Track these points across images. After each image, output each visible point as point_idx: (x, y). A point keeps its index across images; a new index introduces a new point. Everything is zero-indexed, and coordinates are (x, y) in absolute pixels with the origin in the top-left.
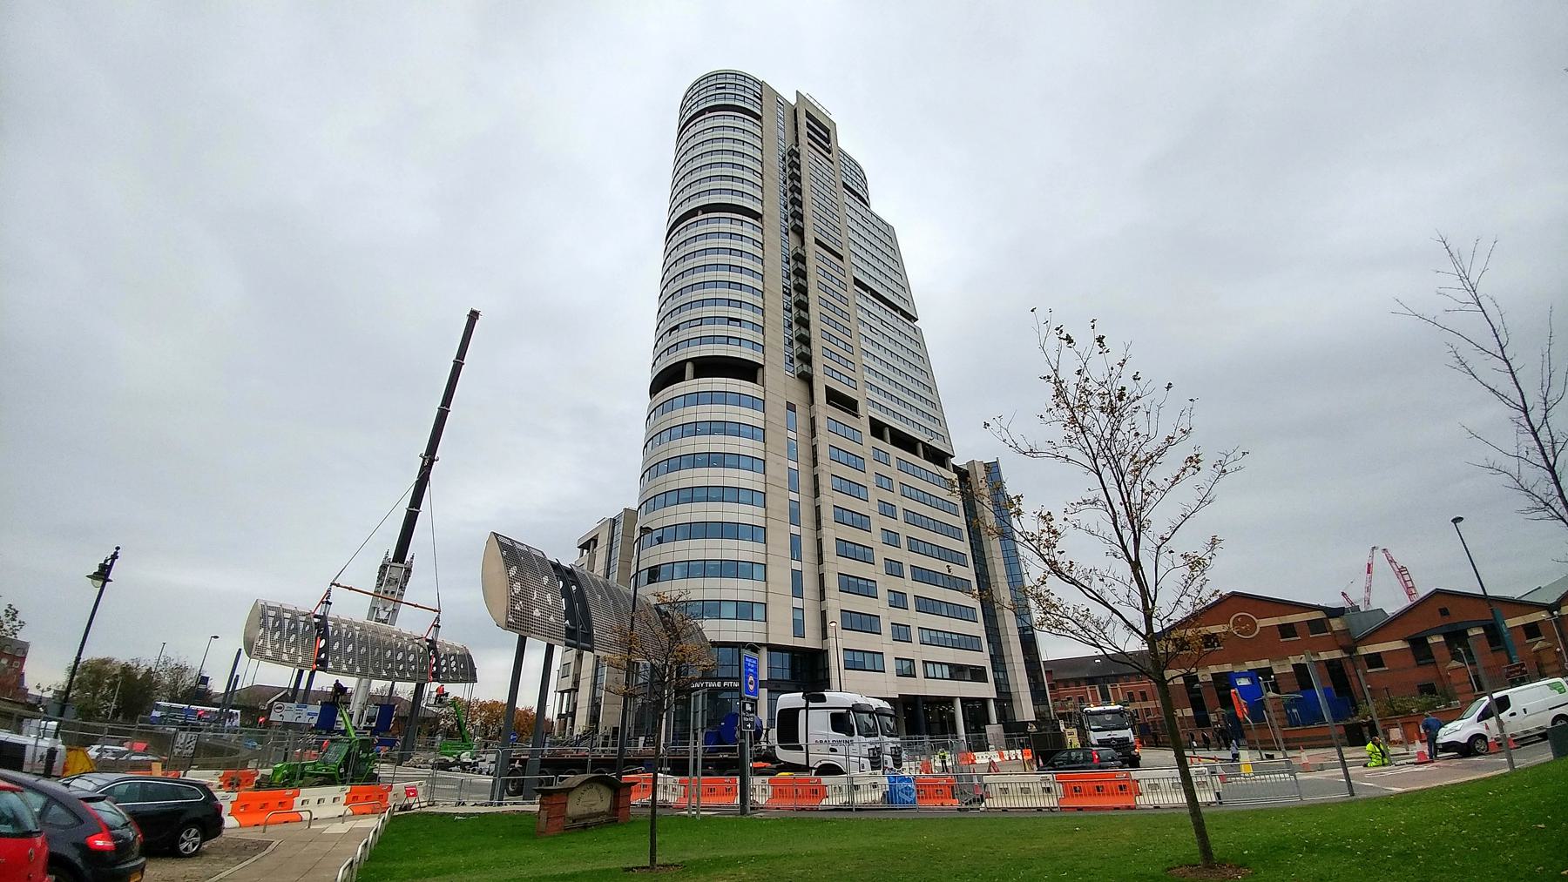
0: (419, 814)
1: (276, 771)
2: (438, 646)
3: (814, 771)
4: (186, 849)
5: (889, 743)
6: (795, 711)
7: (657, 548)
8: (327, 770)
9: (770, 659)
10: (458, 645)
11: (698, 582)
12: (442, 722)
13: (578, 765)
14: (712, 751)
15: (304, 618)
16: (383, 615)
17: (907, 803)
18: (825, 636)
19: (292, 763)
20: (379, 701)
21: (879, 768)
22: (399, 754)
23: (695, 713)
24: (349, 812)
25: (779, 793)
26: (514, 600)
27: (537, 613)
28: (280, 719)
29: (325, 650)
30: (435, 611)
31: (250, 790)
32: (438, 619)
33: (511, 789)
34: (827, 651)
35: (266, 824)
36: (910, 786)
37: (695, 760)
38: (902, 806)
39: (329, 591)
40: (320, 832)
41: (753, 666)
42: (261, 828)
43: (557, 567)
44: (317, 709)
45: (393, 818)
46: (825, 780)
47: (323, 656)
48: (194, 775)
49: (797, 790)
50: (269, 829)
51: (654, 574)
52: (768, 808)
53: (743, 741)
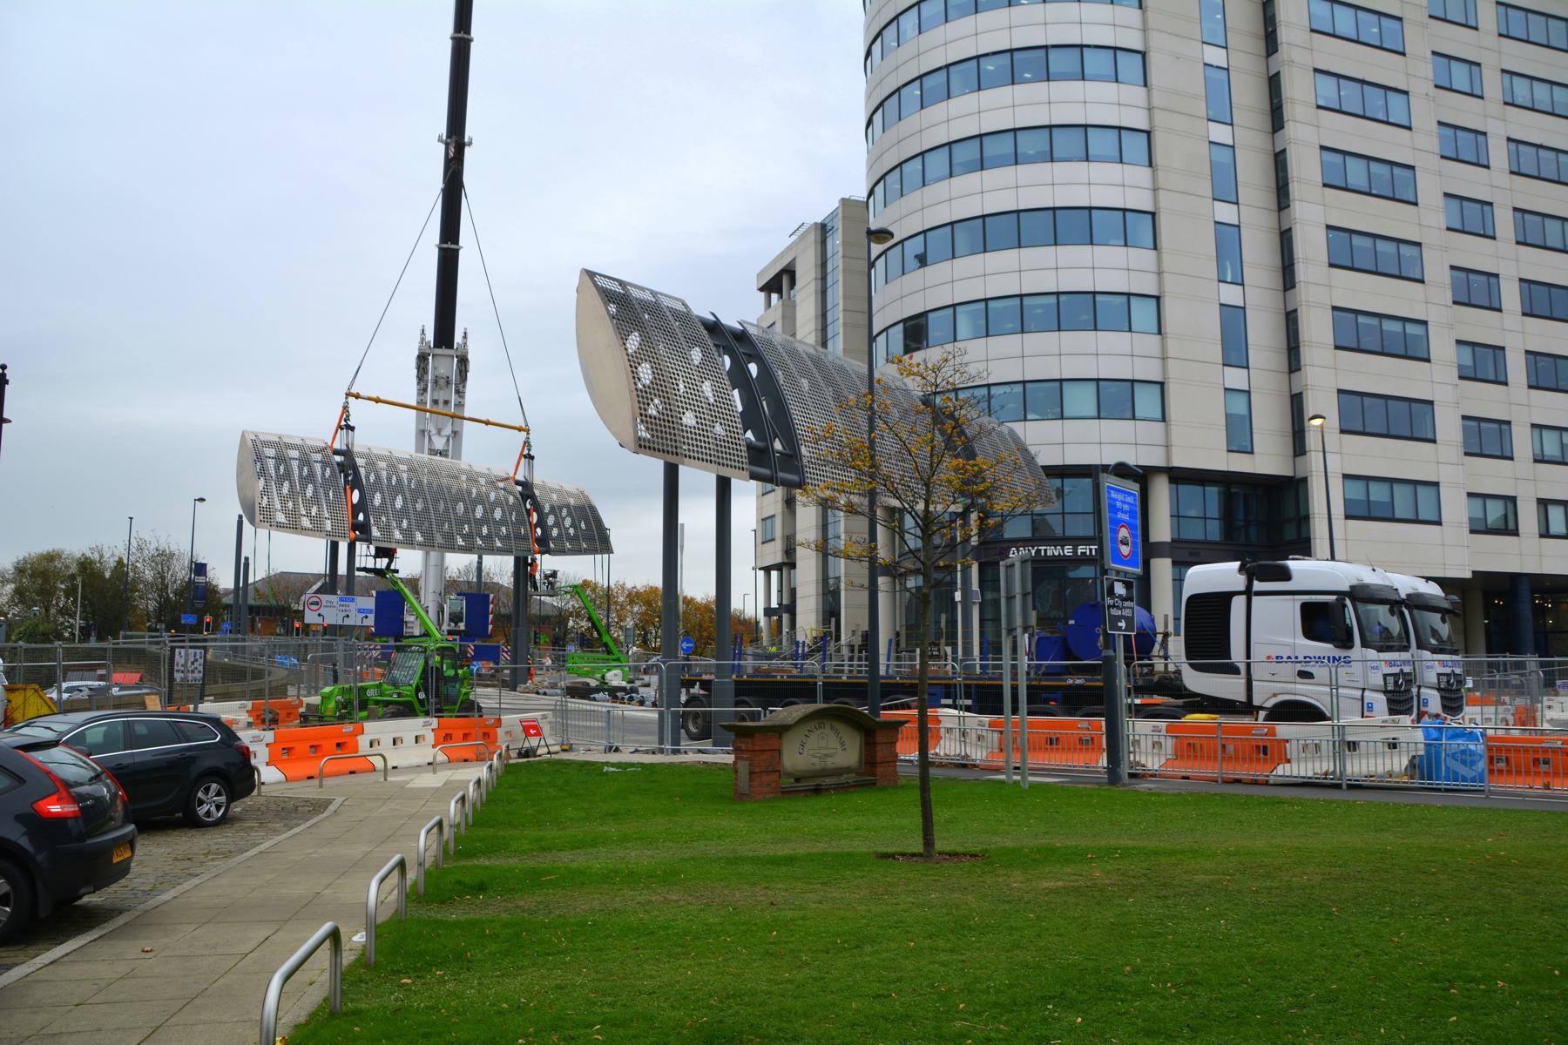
0: (548, 762)
1: (325, 698)
2: (537, 492)
3: (1262, 714)
4: (208, 814)
5: (1432, 667)
6: (1224, 599)
7: (918, 277)
8: (399, 695)
9: (1176, 502)
10: (570, 487)
11: (1010, 343)
12: (571, 623)
13: (799, 690)
14: (1051, 672)
15: (318, 457)
16: (439, 443)
17: (1464, 779)
18: (1299, 444)
19: (347, 686)
20: (465, 589)
21: (1408, 712)
22: (741, 656)
23: (1010, 598)
24: (441, 757)
25: (1187, 749)
26: (643, 396)
27: (689, 419)
28: (319, 620)
29: (362, 506)
30: (520, 429)
31: (296, 727)
32: (527, 443)
33: (693, 729)
34: (1305, 480)
35: (322, 775)
36: (1472, 747)
37: (1015, 689)
38: (1452, 784)
39: (345, 408)
40: (401, 787)
41: (1126, 507)
42: (315, 782)
43: (714, 328)
44: (369, 603)
45: (508, 769)
46: (1284, 730)
47: (361, 517)
48: (208, 707)
49: (1224, 746)
50: (328, 782)
51: (915, 332)
52: (1160, 776)
53: (1111, 652)
